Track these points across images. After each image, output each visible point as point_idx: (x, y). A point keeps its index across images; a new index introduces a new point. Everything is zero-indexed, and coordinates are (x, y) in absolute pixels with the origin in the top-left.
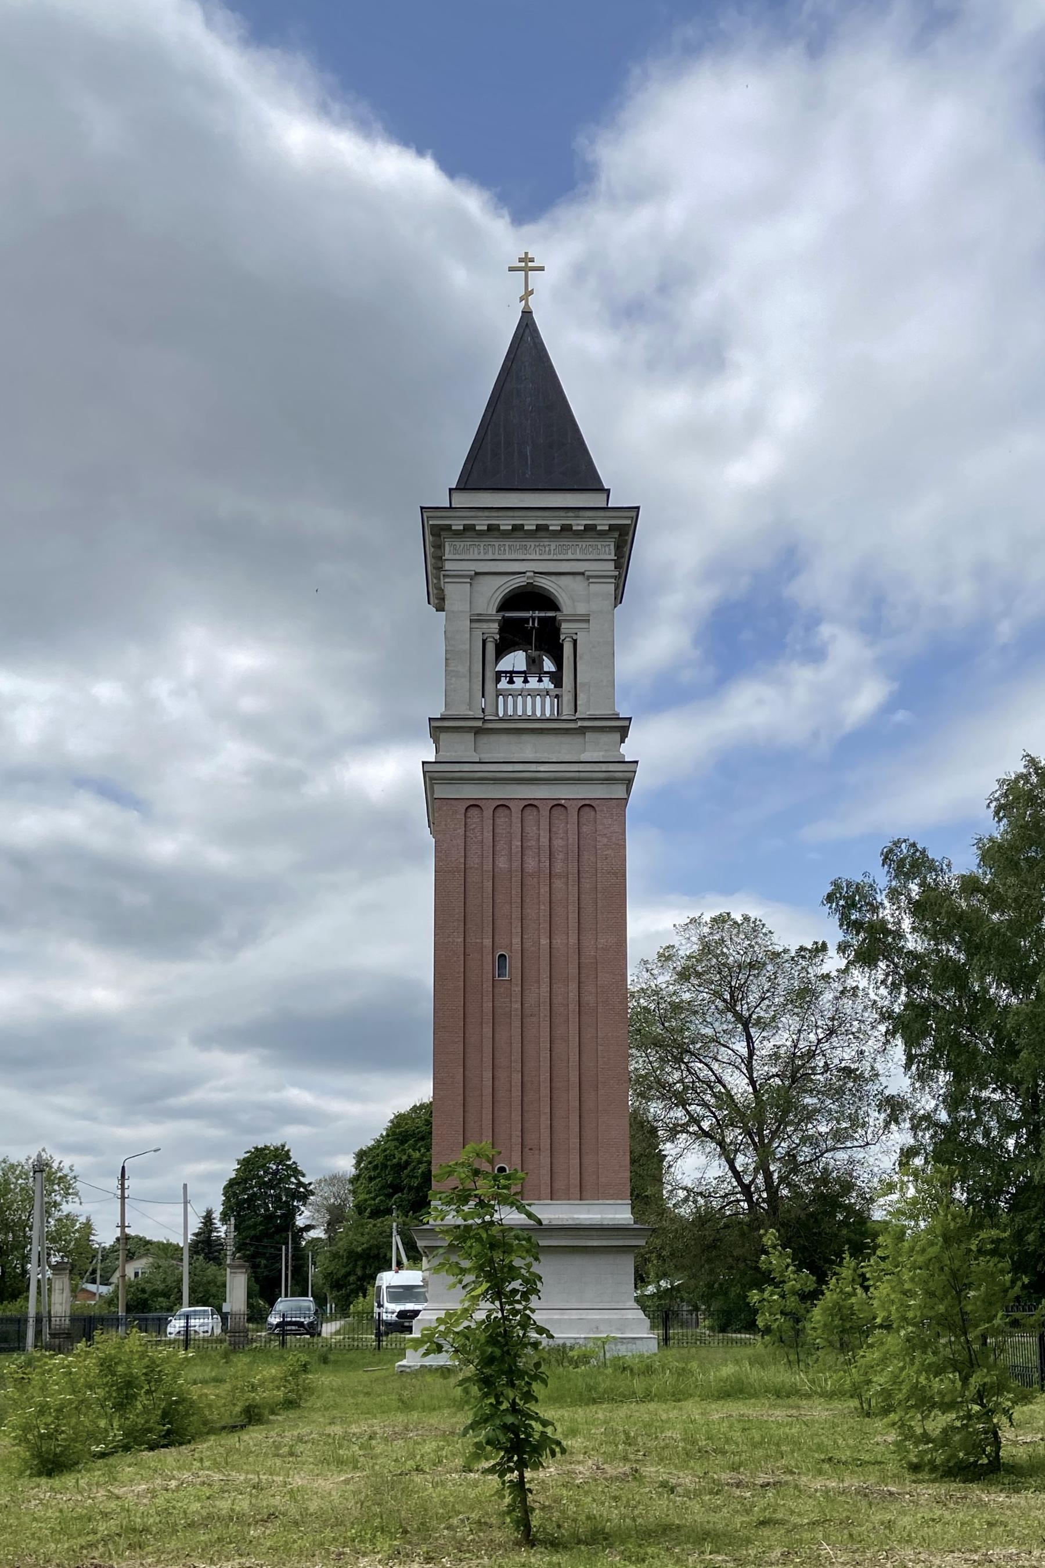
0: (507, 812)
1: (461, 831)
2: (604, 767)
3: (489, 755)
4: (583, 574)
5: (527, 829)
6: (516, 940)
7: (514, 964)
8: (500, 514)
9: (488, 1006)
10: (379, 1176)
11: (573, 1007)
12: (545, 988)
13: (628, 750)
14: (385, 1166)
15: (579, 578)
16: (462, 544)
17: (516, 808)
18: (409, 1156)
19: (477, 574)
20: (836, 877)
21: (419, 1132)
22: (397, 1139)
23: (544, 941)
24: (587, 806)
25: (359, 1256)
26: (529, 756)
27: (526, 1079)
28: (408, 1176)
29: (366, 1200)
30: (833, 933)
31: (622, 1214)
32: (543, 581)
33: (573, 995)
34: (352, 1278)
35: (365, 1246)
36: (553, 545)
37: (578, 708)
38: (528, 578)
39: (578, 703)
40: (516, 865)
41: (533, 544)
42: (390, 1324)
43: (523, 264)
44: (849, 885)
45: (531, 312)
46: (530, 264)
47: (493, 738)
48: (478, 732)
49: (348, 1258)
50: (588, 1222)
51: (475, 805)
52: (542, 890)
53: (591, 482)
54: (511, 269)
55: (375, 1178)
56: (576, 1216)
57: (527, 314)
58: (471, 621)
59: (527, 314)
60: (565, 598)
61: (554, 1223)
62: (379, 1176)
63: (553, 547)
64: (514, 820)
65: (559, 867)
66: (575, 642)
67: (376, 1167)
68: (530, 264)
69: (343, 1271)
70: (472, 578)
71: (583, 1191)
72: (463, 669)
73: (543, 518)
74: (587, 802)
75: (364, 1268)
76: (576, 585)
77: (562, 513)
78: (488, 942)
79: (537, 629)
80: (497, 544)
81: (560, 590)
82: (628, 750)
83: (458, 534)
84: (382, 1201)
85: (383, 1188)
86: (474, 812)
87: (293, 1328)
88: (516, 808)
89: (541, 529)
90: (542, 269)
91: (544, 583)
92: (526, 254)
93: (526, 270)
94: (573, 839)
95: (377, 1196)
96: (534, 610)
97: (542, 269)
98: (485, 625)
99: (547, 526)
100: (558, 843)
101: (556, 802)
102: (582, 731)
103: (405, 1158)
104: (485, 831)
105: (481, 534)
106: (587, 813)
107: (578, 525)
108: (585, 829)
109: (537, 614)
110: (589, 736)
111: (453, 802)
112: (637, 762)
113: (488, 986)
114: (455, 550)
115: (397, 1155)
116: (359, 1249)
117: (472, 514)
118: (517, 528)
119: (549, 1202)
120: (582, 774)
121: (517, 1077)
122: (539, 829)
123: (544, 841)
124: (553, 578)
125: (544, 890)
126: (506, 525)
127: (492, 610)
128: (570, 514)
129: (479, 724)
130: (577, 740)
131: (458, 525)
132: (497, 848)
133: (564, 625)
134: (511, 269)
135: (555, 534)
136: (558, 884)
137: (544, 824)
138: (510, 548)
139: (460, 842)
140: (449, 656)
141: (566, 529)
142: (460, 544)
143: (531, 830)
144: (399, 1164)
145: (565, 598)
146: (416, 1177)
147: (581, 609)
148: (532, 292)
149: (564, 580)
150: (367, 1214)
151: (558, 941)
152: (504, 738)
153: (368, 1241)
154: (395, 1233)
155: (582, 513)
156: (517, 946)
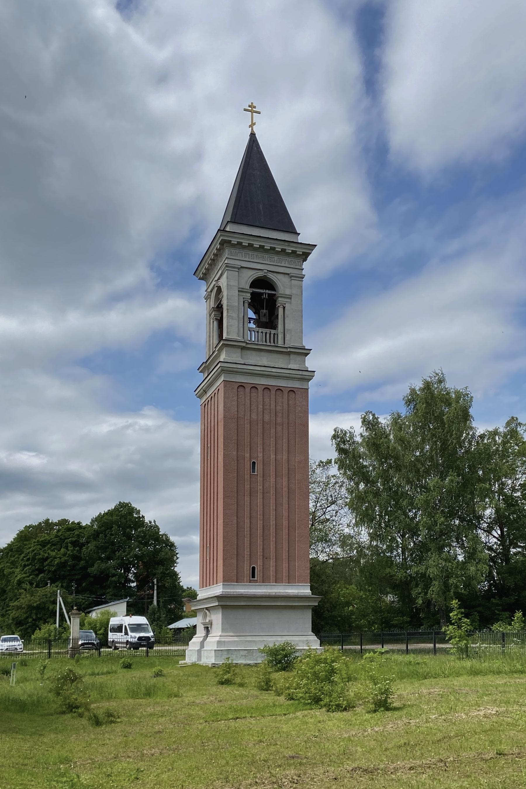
0: (256, 390)
1: (235, 398)
2: (301, 373)
3: (247, 361)
4: (288, 274)
5: (265, 400)
6: (260, 455)
7: (259, 467)
8: (255, 238)
9: (247, 487)
10: (30, 564)
11: (285, 489)
12: (272, 480)
13: (310, 363)
14: (34, 559)
15: (287, 276)
16: (235, 251)
17: (260, 389)
18: (48, 554)
19: (242, 267)
20: (336, 427)
21: (52, 542)
22: (40, 545)
23: (273, 456)
24: (292, 391)
25: (34, 608)
26: (265, 363)
27: (264, 524)
28: (48, 565)
29: (24, 578)
30: (334, 455)
31: (306, 591)
32: (272, 276)
33: (285, 483)
34: (30, 620)
35: (38, 603)
36: (276, 258)
37: (286, 342)
38: (265, 273)
39: (286, 339)
40: (260, 417)
41: (267, 256)
42: (134, 644)
43: (250, 109)
44: (341, 430)
45: (255, 134)
46: (254, 109)
47: (249, 352)
48: (243, 348)
49: (27, 609)
50: (292, 594)
51: (242, 386)
52: (272, 431)
53: (291, 229)
54: (245, 110)
55: (28, 565)
56: (287, 591)
57: (253, 135)
58: (239, 291)
59: (253, 135)
60: (281, 286)
61: (299, 594)
62: (30, 564)
63: (276, 259)
64: (259, 394)
65: (279, 420)
66: (284, 308)
67: (28, 559)
68: (254, 109)
69: (25, 616)
70: (239, 269)
71: (291, 580)
72: (235, 315)
73: (296, 248)
74: (292, 389)
75: (36, 614)
76: (285, 279)
77: (248, 237)
78: (247, 455)
79: (267, 299)
80: (250, 253)
81: (278, 281)
82: (310, 363)
83: (234, 246)
84: (33, 578)
85: (33, 571)
86: (241, 389)
87: (90, 646)
88: (260, 389)
89: (250, 245)
90: (259, 113)
91: (271, 276)
92: (252, 103)
93: (252, 112)
94: (286, 406)
95: (30, 575)
96: (266, 289)
97: (259, 113)
98: (244, 294)
99: (275, 248)
100: (279, 408)
101: (240, 384)
102: (289, 353)
103: (46, 555)
104: (246, 399)
105: (244, 247)
106: (292, 395)
107: (256, 245)
108: (290, 402)
109: (267, 291)
110: (292, 356)
111: (234, 383)
112: (314, 372)
113: (247, 477)
114: (231, 254)
115: (42, 553)
116: (35, 604)
117: (242, 237)
118: (262, 247)
119: (275, 584)
120: (291, 375)
121: (260, 523)
122: (270, 401)
123: (273, 406)
124: (275, 274)
125: (273, 431)
126: (256, 245)
127: (248, 287)
128: (286, 244)
129: (244, 345)
130: (286, 357)
131: (234, 241)
132: (252, 408)
133: (280, 299)
134: (245, 110)
135: (278, 253)
136: (279, 428)
137: (273, 397)
138: (256, 257)
139: (235, 403)
140: (228, 308)
141: (250, 245)
142: (233, 251)
143: (267, 400)
144: (42, 559)
145: (281, 286)
146: (54, 566)
147: (288, 292)
148: (254, 124)
149: (280, 277)
150: (34, 586)
151: (279, 457)
152: (254, 353)
153: (39, 600)
154: (58, 596)
155: (292, 244)
156: (260, 458)
